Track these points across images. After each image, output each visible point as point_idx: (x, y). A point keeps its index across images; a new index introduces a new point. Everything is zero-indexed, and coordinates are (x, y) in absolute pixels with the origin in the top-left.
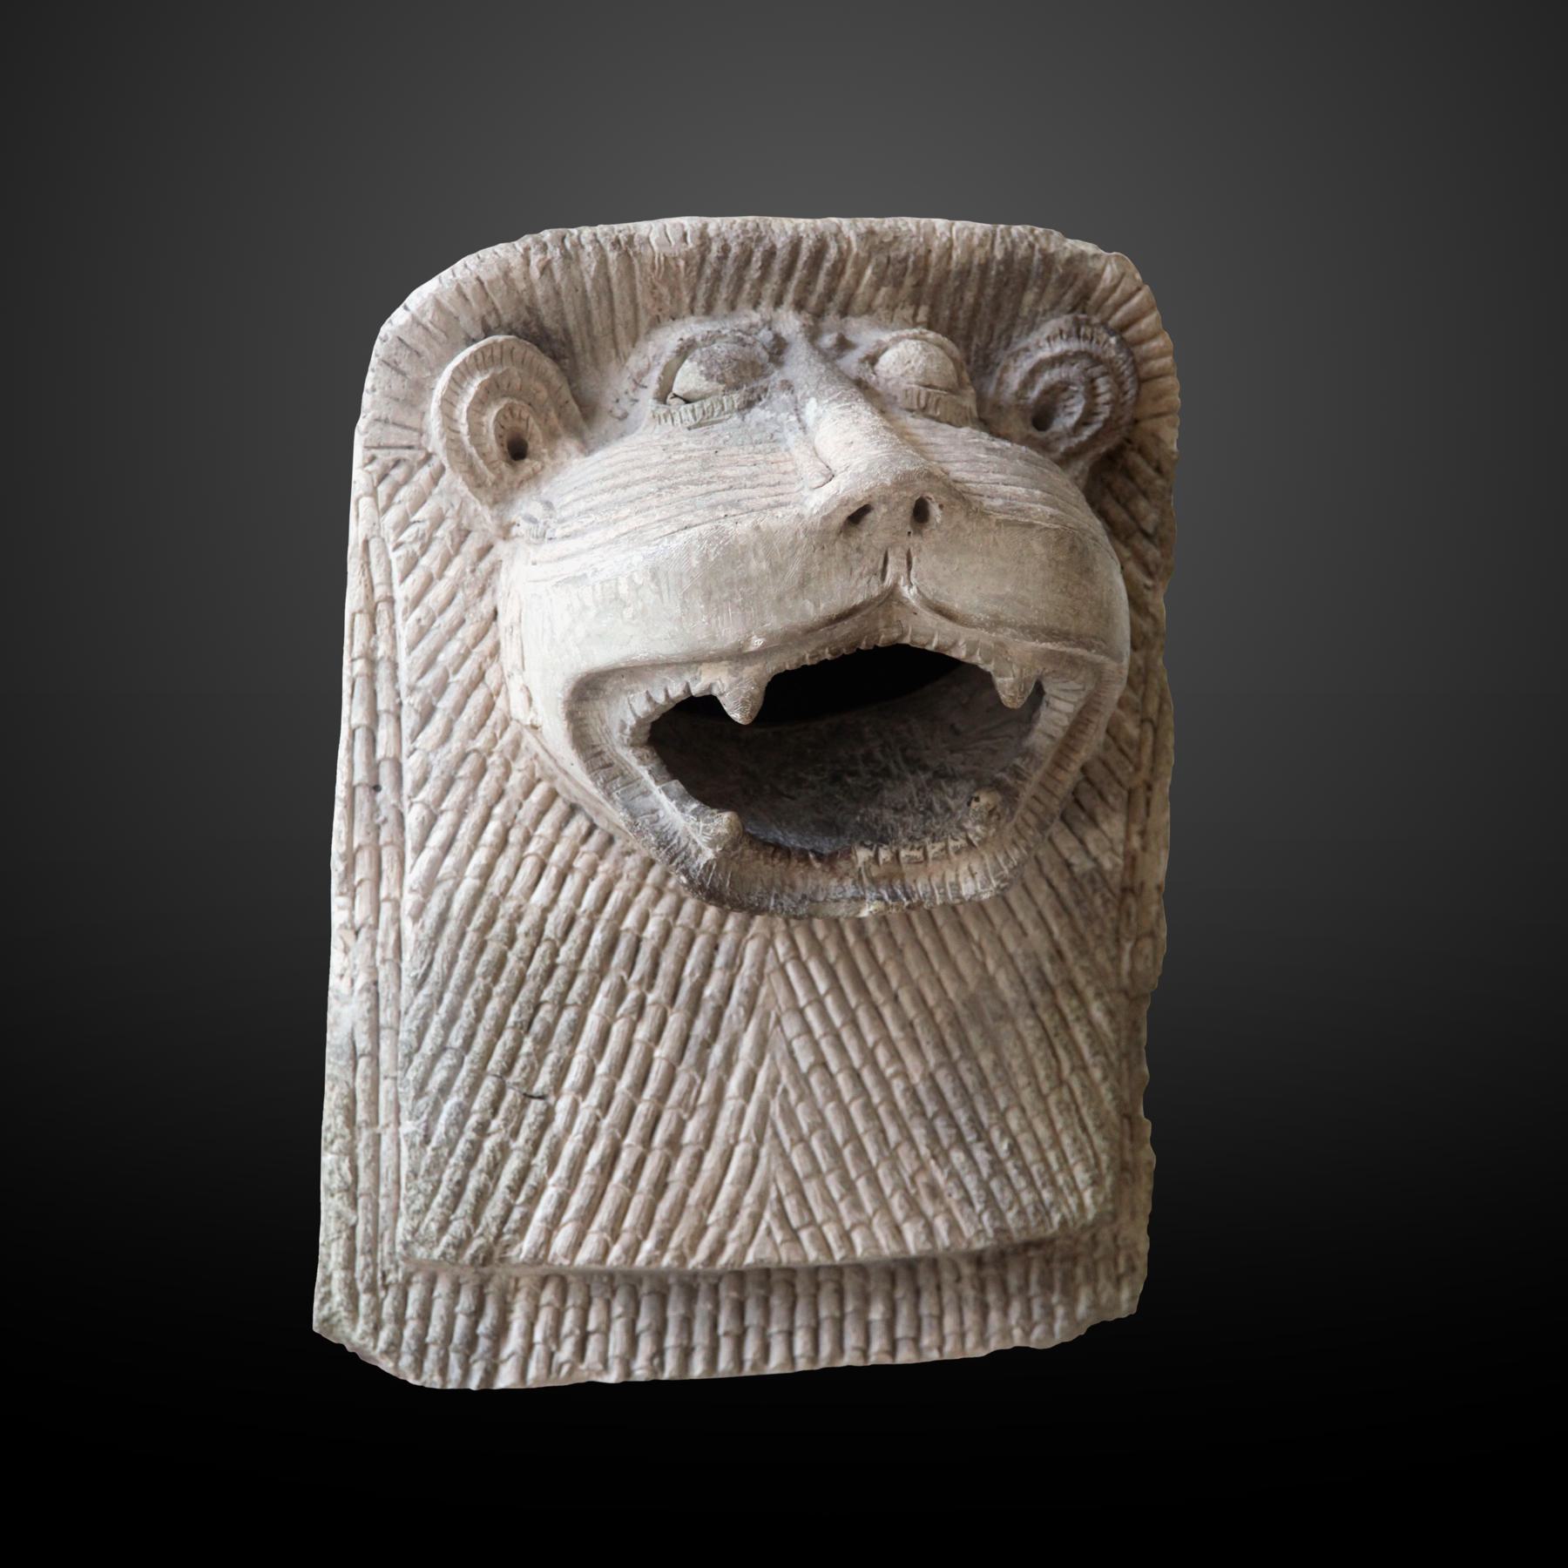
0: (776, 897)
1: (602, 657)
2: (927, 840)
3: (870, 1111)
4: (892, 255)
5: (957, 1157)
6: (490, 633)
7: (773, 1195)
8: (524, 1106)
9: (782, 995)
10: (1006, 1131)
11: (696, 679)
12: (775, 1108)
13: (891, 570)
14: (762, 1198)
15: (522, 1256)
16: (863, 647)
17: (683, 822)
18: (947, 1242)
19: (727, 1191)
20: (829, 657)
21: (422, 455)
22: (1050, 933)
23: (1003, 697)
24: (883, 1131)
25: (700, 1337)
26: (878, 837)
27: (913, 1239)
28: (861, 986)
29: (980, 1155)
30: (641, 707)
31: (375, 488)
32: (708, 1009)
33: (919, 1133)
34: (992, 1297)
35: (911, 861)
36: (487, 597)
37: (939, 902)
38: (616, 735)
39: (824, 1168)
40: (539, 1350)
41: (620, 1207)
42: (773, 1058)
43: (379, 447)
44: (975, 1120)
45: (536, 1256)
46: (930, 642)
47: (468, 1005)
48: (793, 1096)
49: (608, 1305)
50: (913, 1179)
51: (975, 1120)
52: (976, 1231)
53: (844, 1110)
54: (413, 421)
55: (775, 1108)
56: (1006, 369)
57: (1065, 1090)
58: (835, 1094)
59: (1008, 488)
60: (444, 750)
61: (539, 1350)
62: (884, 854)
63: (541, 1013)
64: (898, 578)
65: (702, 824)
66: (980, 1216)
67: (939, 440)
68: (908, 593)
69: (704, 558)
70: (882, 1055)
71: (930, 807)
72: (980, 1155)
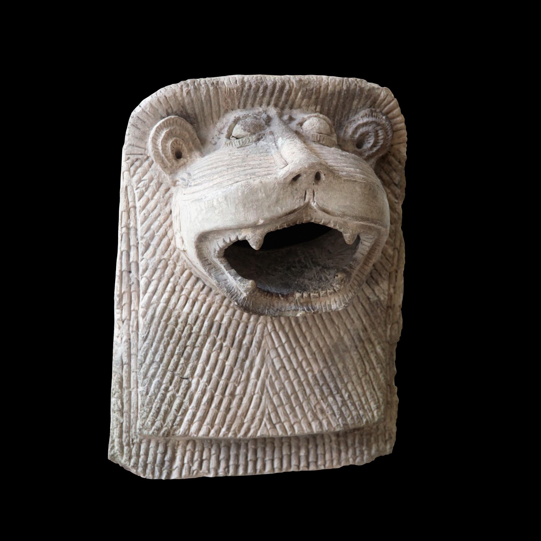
0: (268, 309)
1: (208, 227)
2: (320, 290)
3: (300, 383)
4: (308, 88)
5: (330, 399)
6: (169, 219)
7: (267, 412)
8: (181, 381)
9: (270, 343)
10: (347, 390)
11: (240, 234)
12: (267, 382)
13: (307, 197)
14: (263, 413)
15: (180, 433)
16: (298, 223)
17: (236, 284)
18: (327, 429)
19: (251, 411)
20: (286, 227)
21: (145, 157)
22: (362, 322)
23: (346, 240)
24: (305, 390)
25: (242, 461)
26: (303, 289)
27: (315, 427)
28: (297, 340)
29: (338, 398)
30: (221, 244)
31: (129, 169)
32: (244, 348)
33: (317, 391)
34: (342, 448)
35: (314, 297)
36: (168, 206)
37: (324, 311)
38: (213, 254)
39: (284, 403)
40: (186, 466)
41: (214, 416)
42: (267, 365)
43: (131, 154)
44: (336, 386)
45: (185, 433)
46: (321, 222)
47: (162, 347)
48: (274, 378)
49: (210, 450)
50: (315, 407)
51: (336, 386)
52: (337, 425)
53: (291, 383)
54: (142, 145)
55: (267, 382)
56: (347, 127)
57: (367, 376)
58: (288, 377)
59: (348, 169)
60: (153, 259)
61: (186, 466)
62: (305, 295)
63: (187, 350)
64: (310, 199)
65: (242, 284)
66: (338, 419)
67: (324, 152)
68: (313, 205)
69: (243, 193)
70: (304, 364)
71: (321, 278)
72: (338, 398)
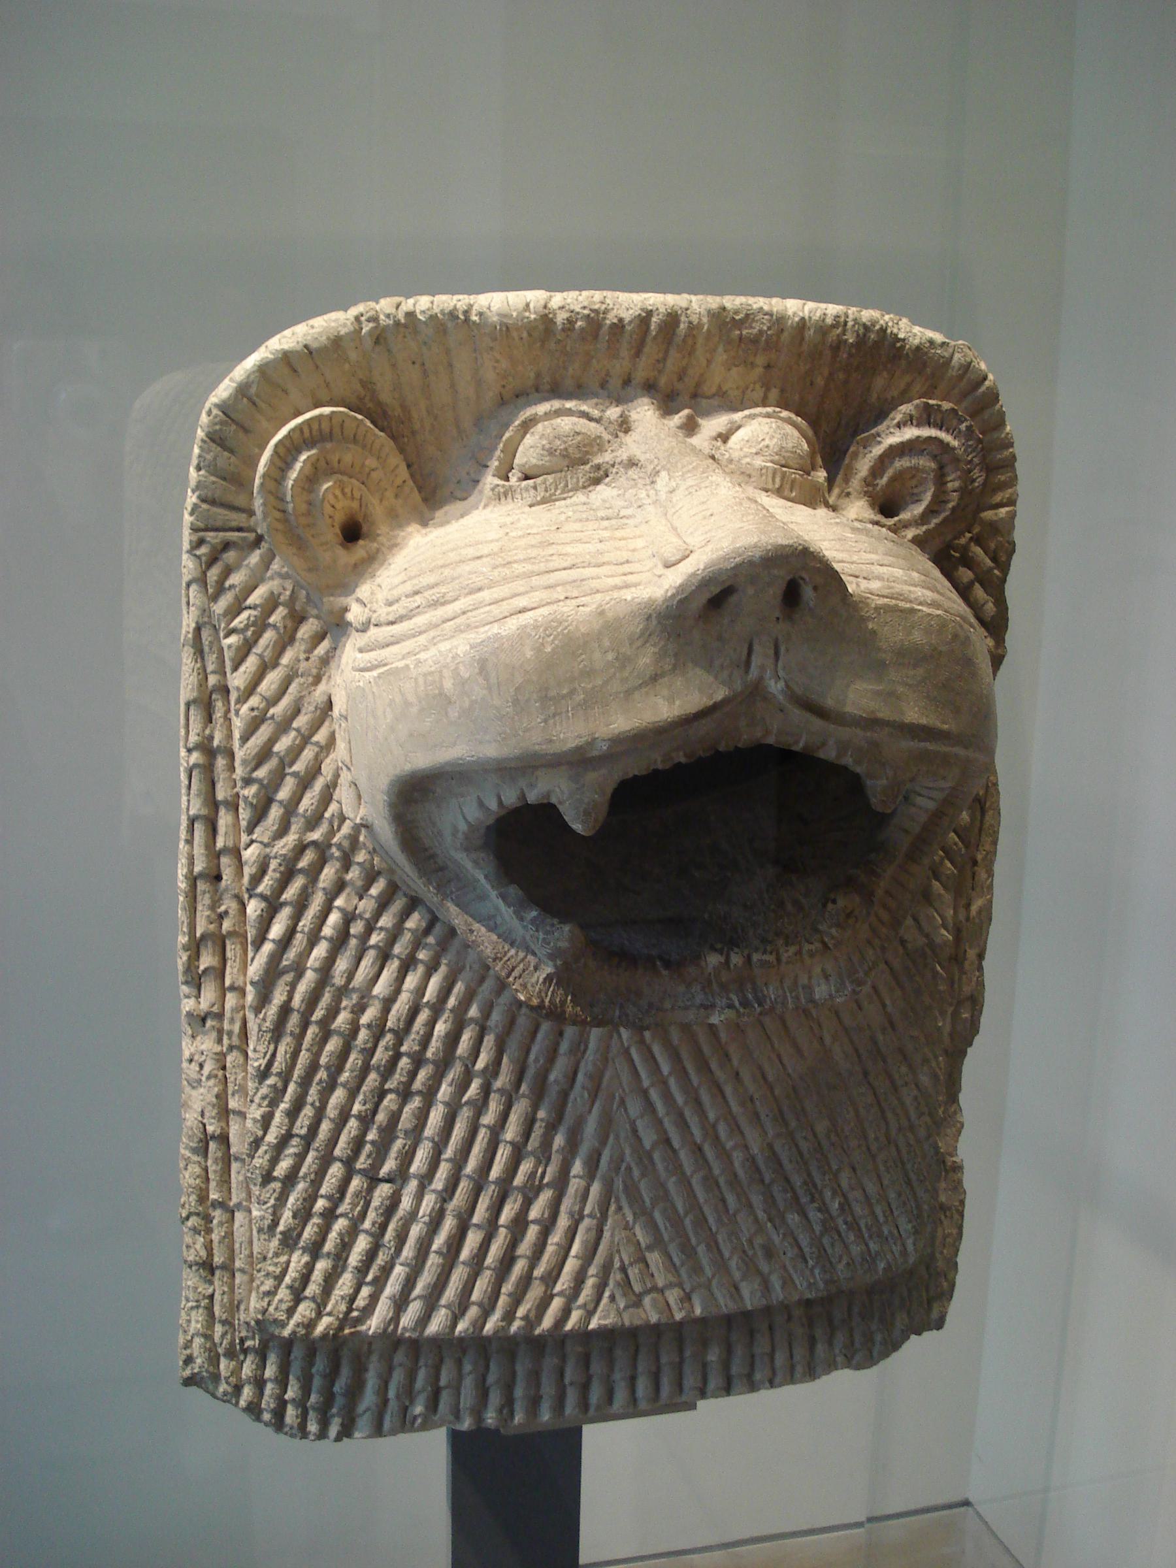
0: (622, 1006)
1: (422, 760)
2: (780, 942)
3: (710, 1182)
4: (744, 332)
5: (793, 1218)
6: (327, 724)
7: (617, 1264)
8: (371, 1190)
9: (625, 1077)
10: (837, 1191)
11: (532, 786)
12: (619, 1184)
13: (756, 661)
14: (606, 1269)
15: (371, 1332)
16: (722, 748)
17: (521, 931)
18: (781, 1297)
19: (571, 1265)
20: (683, 760)
21: (251, 536)
22: (884, 1006)
23: (873, 800)
24: (723, 1200)
25: (548, 1389)
26: (731, 940)
27: (750, 1297)
28: (704, 1066)
29: (815, 1216)
30: (473, 813)
31: (204, 573)
32: (553, 1092)
33: (757, 1200)
34: (819, 1333)
35: (764, 964)
36: (322, 687)
37: (790, 1006)
38: (448, 839)
39: (666, 1237)
40: (393, 1405)
41: (467, 1282)
42: (617, 1137)
43: (206, 530)
44: (810, 1183)
45: (385, 1330)
46: (797, 742)
47: (313, 1095)
48: (636, 1173)
49: (459, 1363)
50: (750, 1241)
51: (810, 1183)
52: (807, 1283)
53: (685, 1182)
54: (240, 501)
55: (619, 1184)
56: (856, 455)
57: (893, 1150)
58: (678, 1168)
59: (884, 569)
60: (280, 843)
61: (393, 1405)
62: (736, 959)
63: (385, 1102)
64: (762, 668)
65: (541, 936)
66: (812, 1270)
67: (799, 520)
68: (775, 687)
69: (539, 649)
70: (722, 1130)
71: (781, 904)
72: (815, 1216)
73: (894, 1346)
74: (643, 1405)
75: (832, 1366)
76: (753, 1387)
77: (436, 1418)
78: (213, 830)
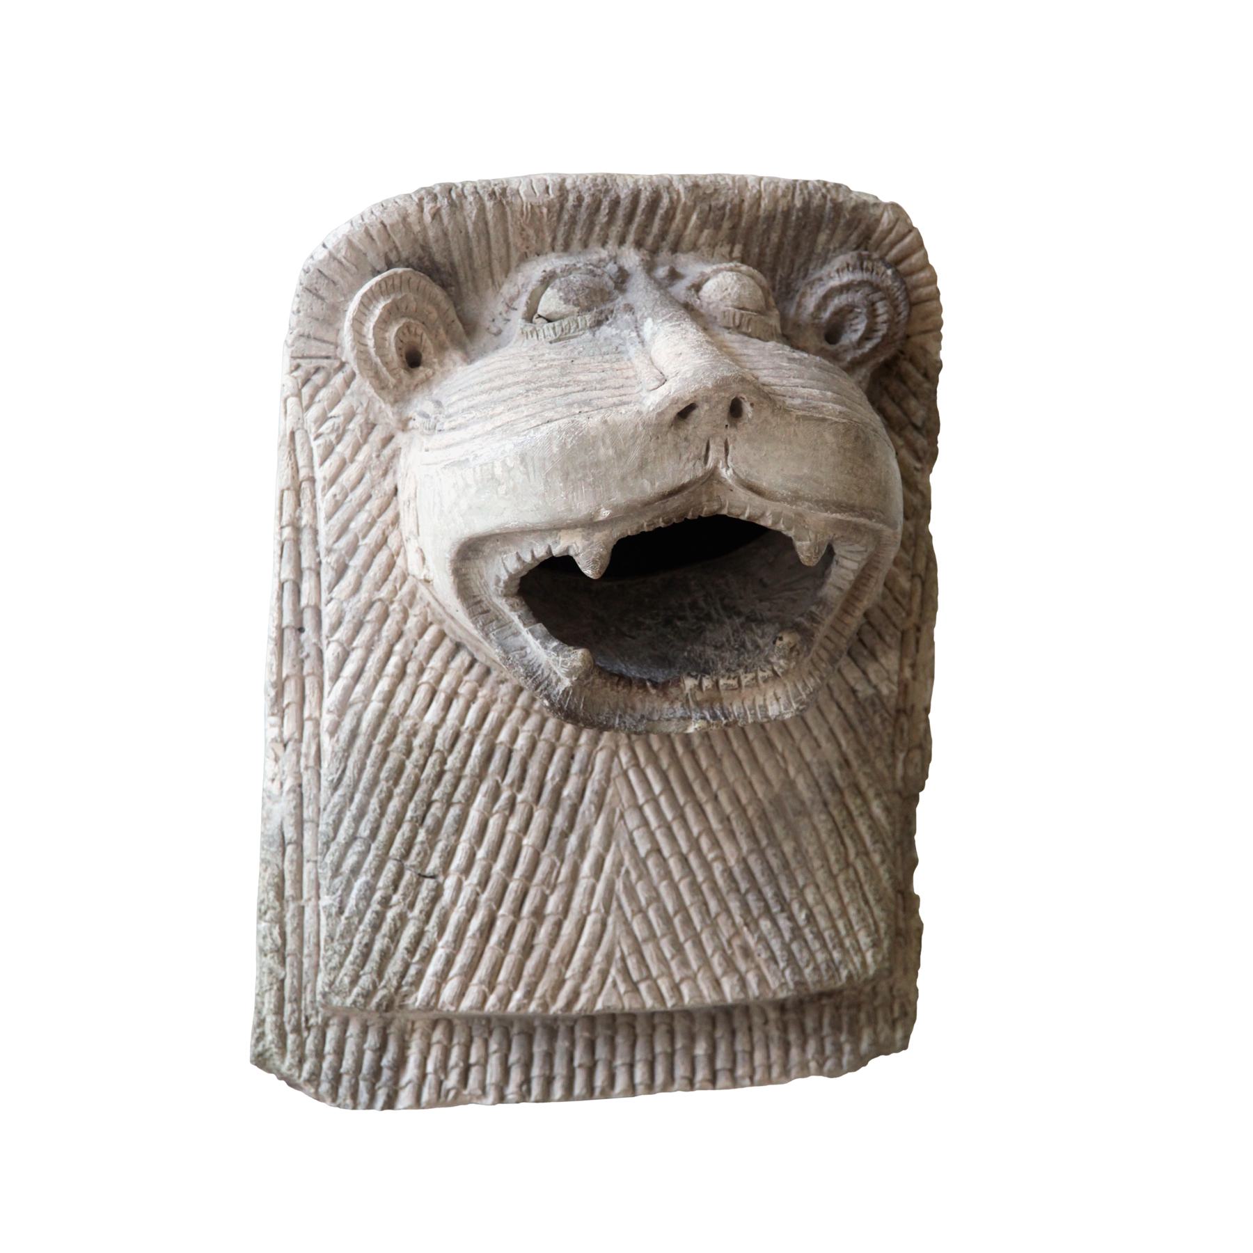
0: (620, 717)
1: (481, 525)
2: (741, 671)
3: (695, 888)
4: (713, 203)
5: (765, 924)
6: (392, 506)
7: (618, 955)
8: (419, 883)
9: (625, 795)
10: (804, 904)
11: (556, 543)
12: (619, 885)
13: (712, 455)
14: (609, 957)
15: (417, 1004)
16: (689, 517)
17: (545, 657)
18: (757, 993)
19: (581, 952)
20: (662, 525)
21: (337, 364)
22: (839, 745)
23: (802, 557)
24: (705, 904)
26: (702, 669)
27: (730, 990)
28: (688, 788)
29: (783, 923)
30: (512, 565)
31: (300, 390)
32: (565, 806)
33: (734, 905)
34: (793, 1037)
35: (728, 688)
36: (389, 477)
37: (750, 721)
38: (492, 587)
39: (659, 933)
40: (431, 1079)
41: (495, 964)
42: (618, 845)
43: (303, 357)
44: (779, 895)
45: (428, 1003)
46: (743, 513)
47: (374, 803)
48: (634, 876)
49: (486, 1043)
50: (729, 942)
51: (779, 895)
52: (780, 984)
53: (674, 887)
54: (330, 336)
55: (619, 885)
56: (804, 295)
57: (851, 871)
58: (668, 874)
59: (806, 390)
60: (355, 600)
61: (431, 1079)
62: (707, 683)
63: (433, 810)
64: (717, 462)
65: (561, 659)
66: (783, 972)
67: (750, 352)
68: (726, 474)
69: (563, 446)
70: (705, 843)
71: (743, 645)
72: (783, 923)
73: (860, 1062)
74: (640, 1088)
75: (804, 1072)
76: (735, 1083)
77: (466, 1092)
78: (297, 592)
